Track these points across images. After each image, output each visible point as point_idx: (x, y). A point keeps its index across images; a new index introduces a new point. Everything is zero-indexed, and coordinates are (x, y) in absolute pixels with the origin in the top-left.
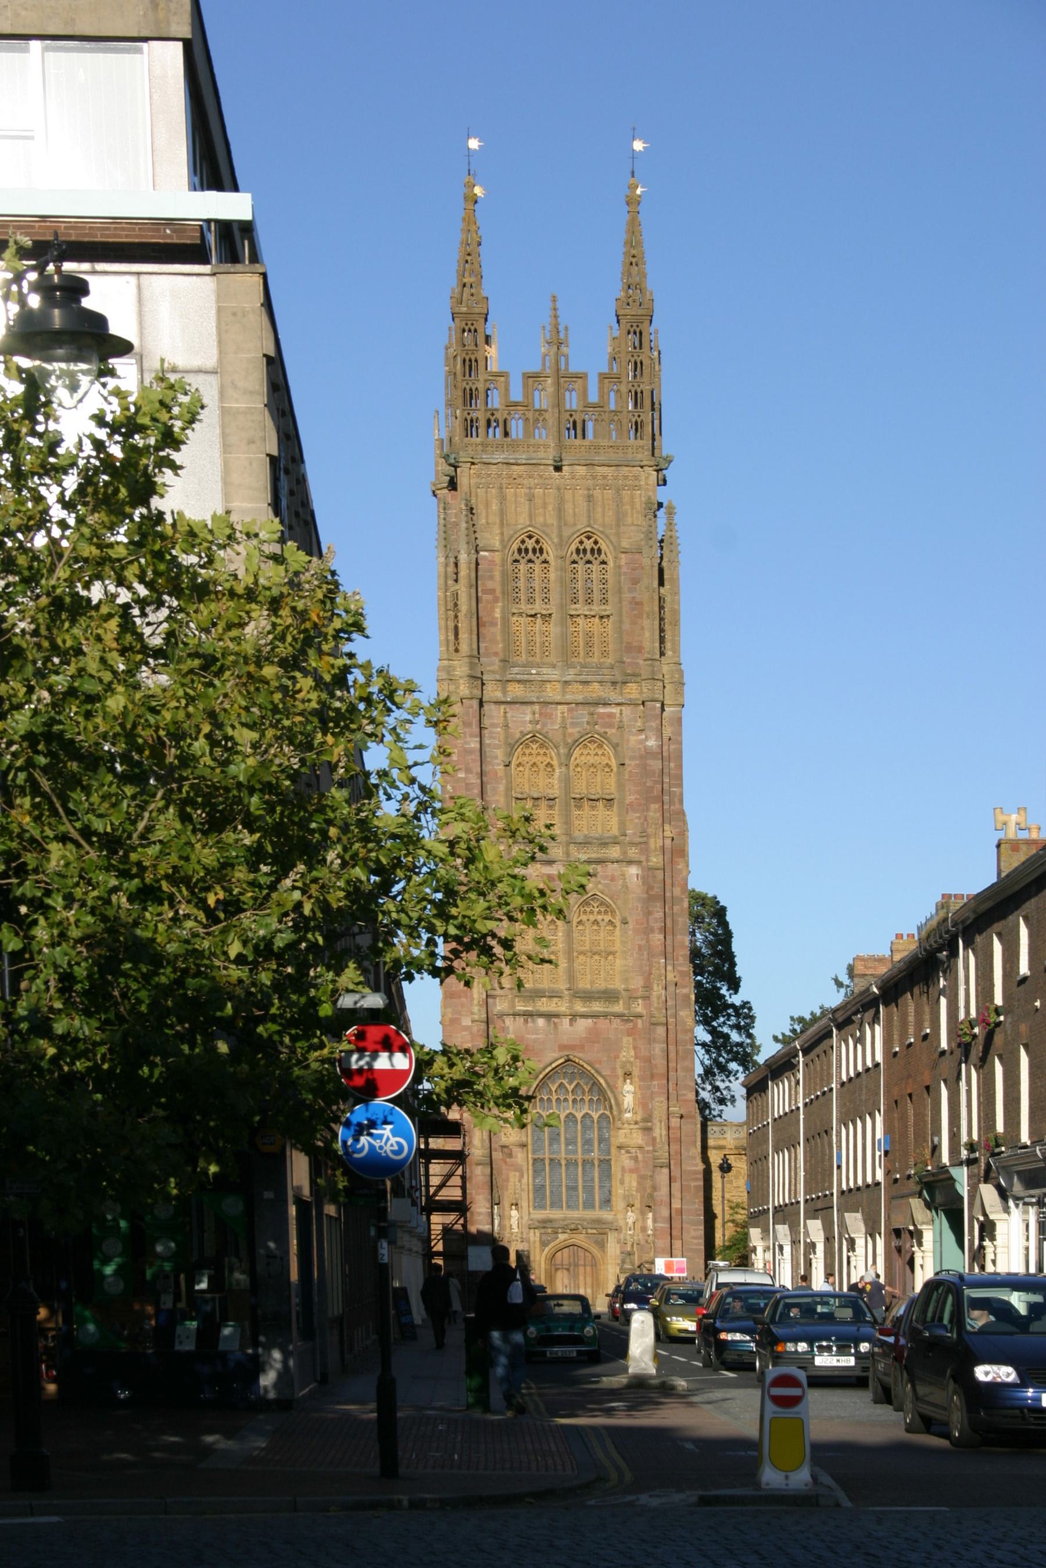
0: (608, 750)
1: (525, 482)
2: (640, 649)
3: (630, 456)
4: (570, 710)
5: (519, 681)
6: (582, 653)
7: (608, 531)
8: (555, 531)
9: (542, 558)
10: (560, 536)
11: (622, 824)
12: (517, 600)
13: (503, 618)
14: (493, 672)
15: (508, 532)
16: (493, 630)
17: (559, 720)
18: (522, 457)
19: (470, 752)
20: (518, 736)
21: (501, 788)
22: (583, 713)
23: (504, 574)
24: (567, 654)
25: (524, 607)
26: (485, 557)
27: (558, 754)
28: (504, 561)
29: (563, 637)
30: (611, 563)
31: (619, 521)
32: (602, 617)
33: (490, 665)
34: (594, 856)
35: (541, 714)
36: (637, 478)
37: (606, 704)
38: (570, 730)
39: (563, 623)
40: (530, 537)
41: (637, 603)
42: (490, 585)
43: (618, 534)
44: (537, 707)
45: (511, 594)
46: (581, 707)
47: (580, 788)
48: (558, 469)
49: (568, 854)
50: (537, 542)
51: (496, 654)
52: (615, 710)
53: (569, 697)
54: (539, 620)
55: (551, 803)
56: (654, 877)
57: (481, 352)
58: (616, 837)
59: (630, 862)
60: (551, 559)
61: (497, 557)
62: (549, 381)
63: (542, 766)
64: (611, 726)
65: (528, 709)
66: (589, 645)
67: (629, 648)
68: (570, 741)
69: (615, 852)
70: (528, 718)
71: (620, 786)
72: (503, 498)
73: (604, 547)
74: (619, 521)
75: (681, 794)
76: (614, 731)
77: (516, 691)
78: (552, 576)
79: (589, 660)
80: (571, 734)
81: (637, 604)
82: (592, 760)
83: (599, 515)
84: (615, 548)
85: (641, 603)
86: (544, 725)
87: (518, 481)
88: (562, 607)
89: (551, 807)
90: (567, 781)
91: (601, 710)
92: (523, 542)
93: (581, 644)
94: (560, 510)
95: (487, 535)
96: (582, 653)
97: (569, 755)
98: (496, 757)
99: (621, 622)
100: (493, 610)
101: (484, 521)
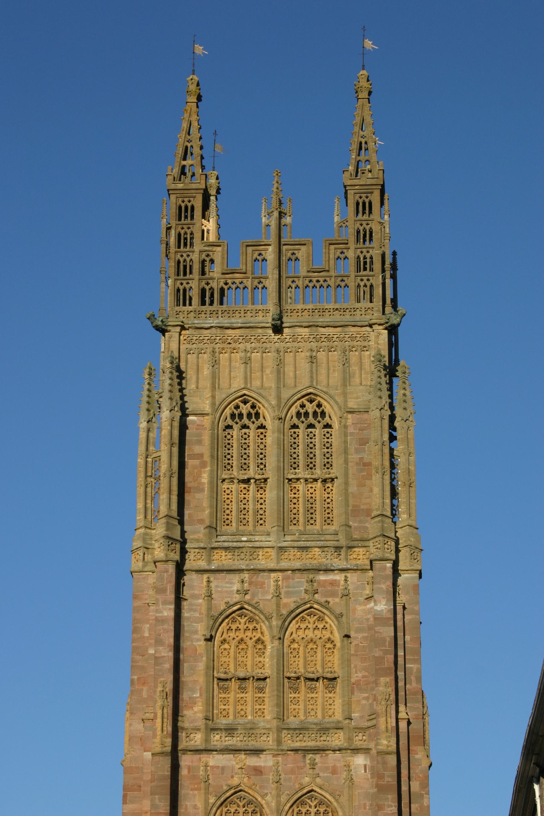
0: (330, 621)
1: (241, 346)
2: (368, 512)
3: (358, 318)
4: (285, 578)
5: (226, 549)
6: (301, 520)
7: (332, 392)
8: (273, 393)
9: (258, 423)
10: (279, 398)
11: (348, 705)
12: (229, 467)
13: (211, 482)
14: (198, 541)
15: (219, 397)
16: (198, 496)
17: (272, 589)
18: (237, 321)
19: (160, 621)
20: (223, 607)
21: (201, 666)
22: (301, 580)
23: (215, 441)
24: (285, 522)
25: (235, 473)
26: (193, 422)
27: (271, 627)
28: (214, 426)
29: (281, 501)
30: (336, 425)
31: (346, 380)
32: (325, 481)
33: (194, 533)
34: (311, 744)
35: (250, 583)
36: (365, 338)
37: (327, 570)
38: (285, 600)
39: (281, 487)
40: (245, 402)
41: (365, 465)
42: (197, 449)
43: (345, 394)
44: (246, 576)
45: (220, 457)
46: (298, 574)
47: (298, 666)
48: (278, 329)
49: (279, 742)
50: (253, 407)
51: (201, 521)
52: (339, 577)
53: (284, 564)
54: (252, 487)
55: (261, 684)
56: (385, 763)
57: (198, 225)
58: (339, 722)
59: (356, 751)
60: (269, 424)
61: (207, 421)
62: (270, 249)
63: (250, 643)
64: (333, 594)
65: (236, 578)
66: (310, 511)
67: (356, 512)
68: (285, 612)
69: (338, 739)
70: (236, 586)
71: (346, 662)
72: (215, 363)
73: (327, 408)
74: (346, 380)
75: (419, 671)
76: (337, 600)
77: (222, 559)
78: (270, 440)
79: (309, 527)
80: (286, 605)
81: (365, 465)
82: (310, 634)
83: (322, 377)
84: (340, 408)
85: (369, 464)
86: (253, 595)
87: (233, 345)
88: (281, 470)
89: (261, 690)
90: (281, 658)
91: (322, 577)
92: (237, 407)
93: (301, 510)
94: (279, 372)
95: (195, 399)
96: (301, 520)
97: (284, 628)
98: (196, 632)
99: (346, 483)
100: (199, 475)
101: (193, 386)
